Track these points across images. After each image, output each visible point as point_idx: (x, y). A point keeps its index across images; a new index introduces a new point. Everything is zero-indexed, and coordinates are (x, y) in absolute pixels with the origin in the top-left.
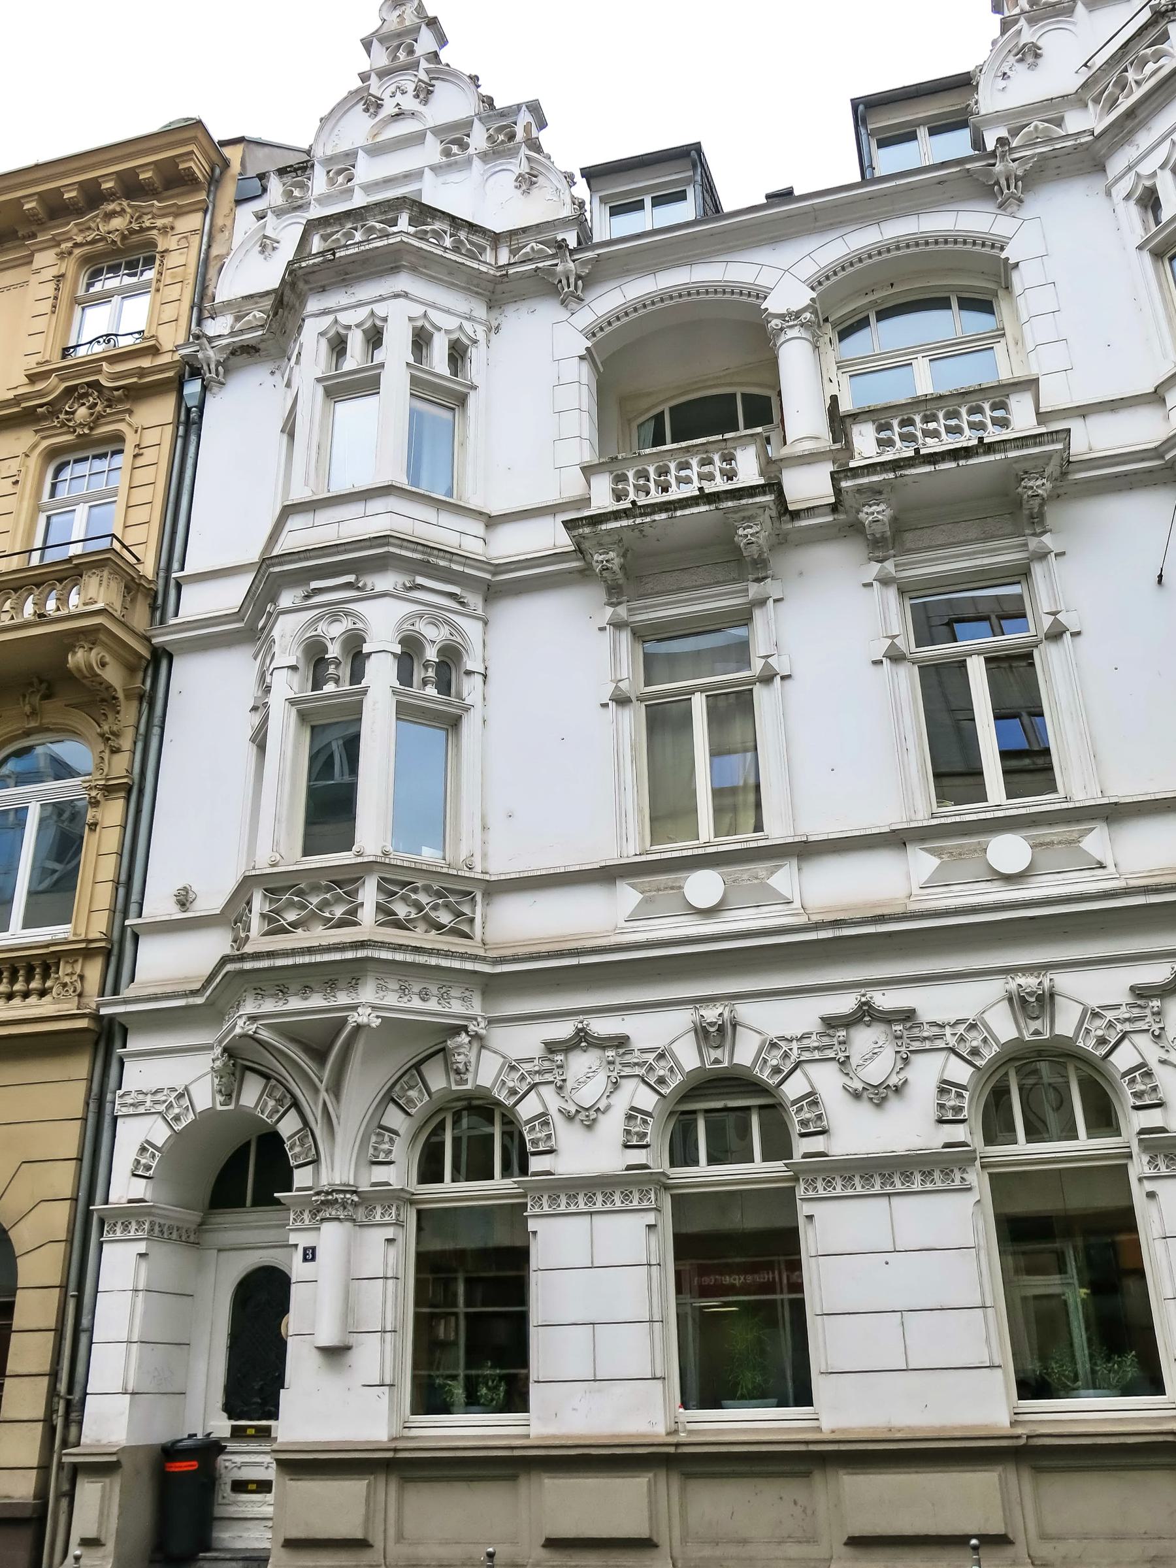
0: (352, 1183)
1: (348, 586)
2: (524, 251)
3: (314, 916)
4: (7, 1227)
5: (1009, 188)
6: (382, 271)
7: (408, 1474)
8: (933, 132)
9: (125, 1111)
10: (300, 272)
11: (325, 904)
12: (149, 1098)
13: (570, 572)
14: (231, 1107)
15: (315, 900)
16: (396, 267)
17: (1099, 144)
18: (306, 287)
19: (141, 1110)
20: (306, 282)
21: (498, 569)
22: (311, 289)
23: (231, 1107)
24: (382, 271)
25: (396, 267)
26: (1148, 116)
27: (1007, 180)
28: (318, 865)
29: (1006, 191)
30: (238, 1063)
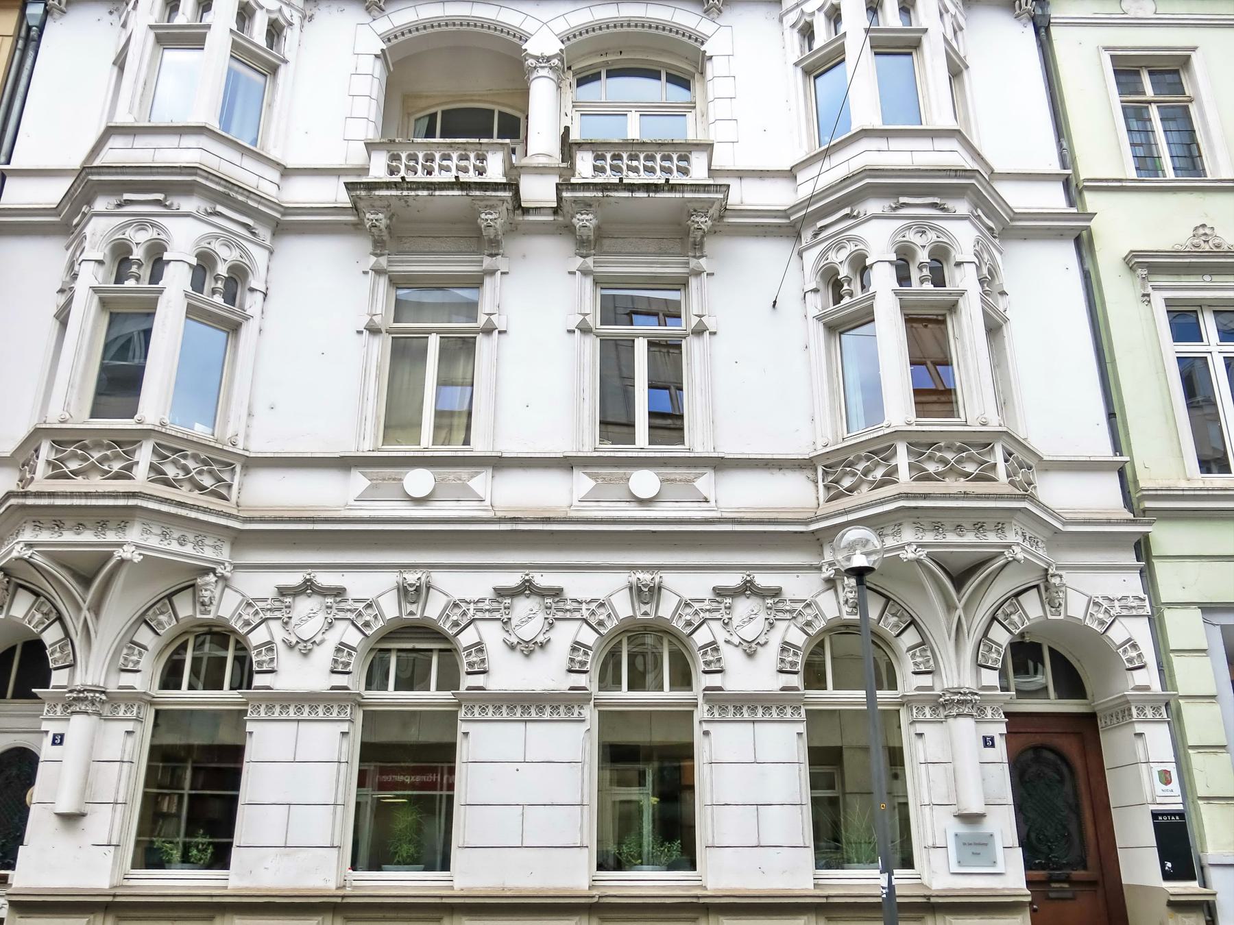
7: (121, 914)
15: (96, 455)
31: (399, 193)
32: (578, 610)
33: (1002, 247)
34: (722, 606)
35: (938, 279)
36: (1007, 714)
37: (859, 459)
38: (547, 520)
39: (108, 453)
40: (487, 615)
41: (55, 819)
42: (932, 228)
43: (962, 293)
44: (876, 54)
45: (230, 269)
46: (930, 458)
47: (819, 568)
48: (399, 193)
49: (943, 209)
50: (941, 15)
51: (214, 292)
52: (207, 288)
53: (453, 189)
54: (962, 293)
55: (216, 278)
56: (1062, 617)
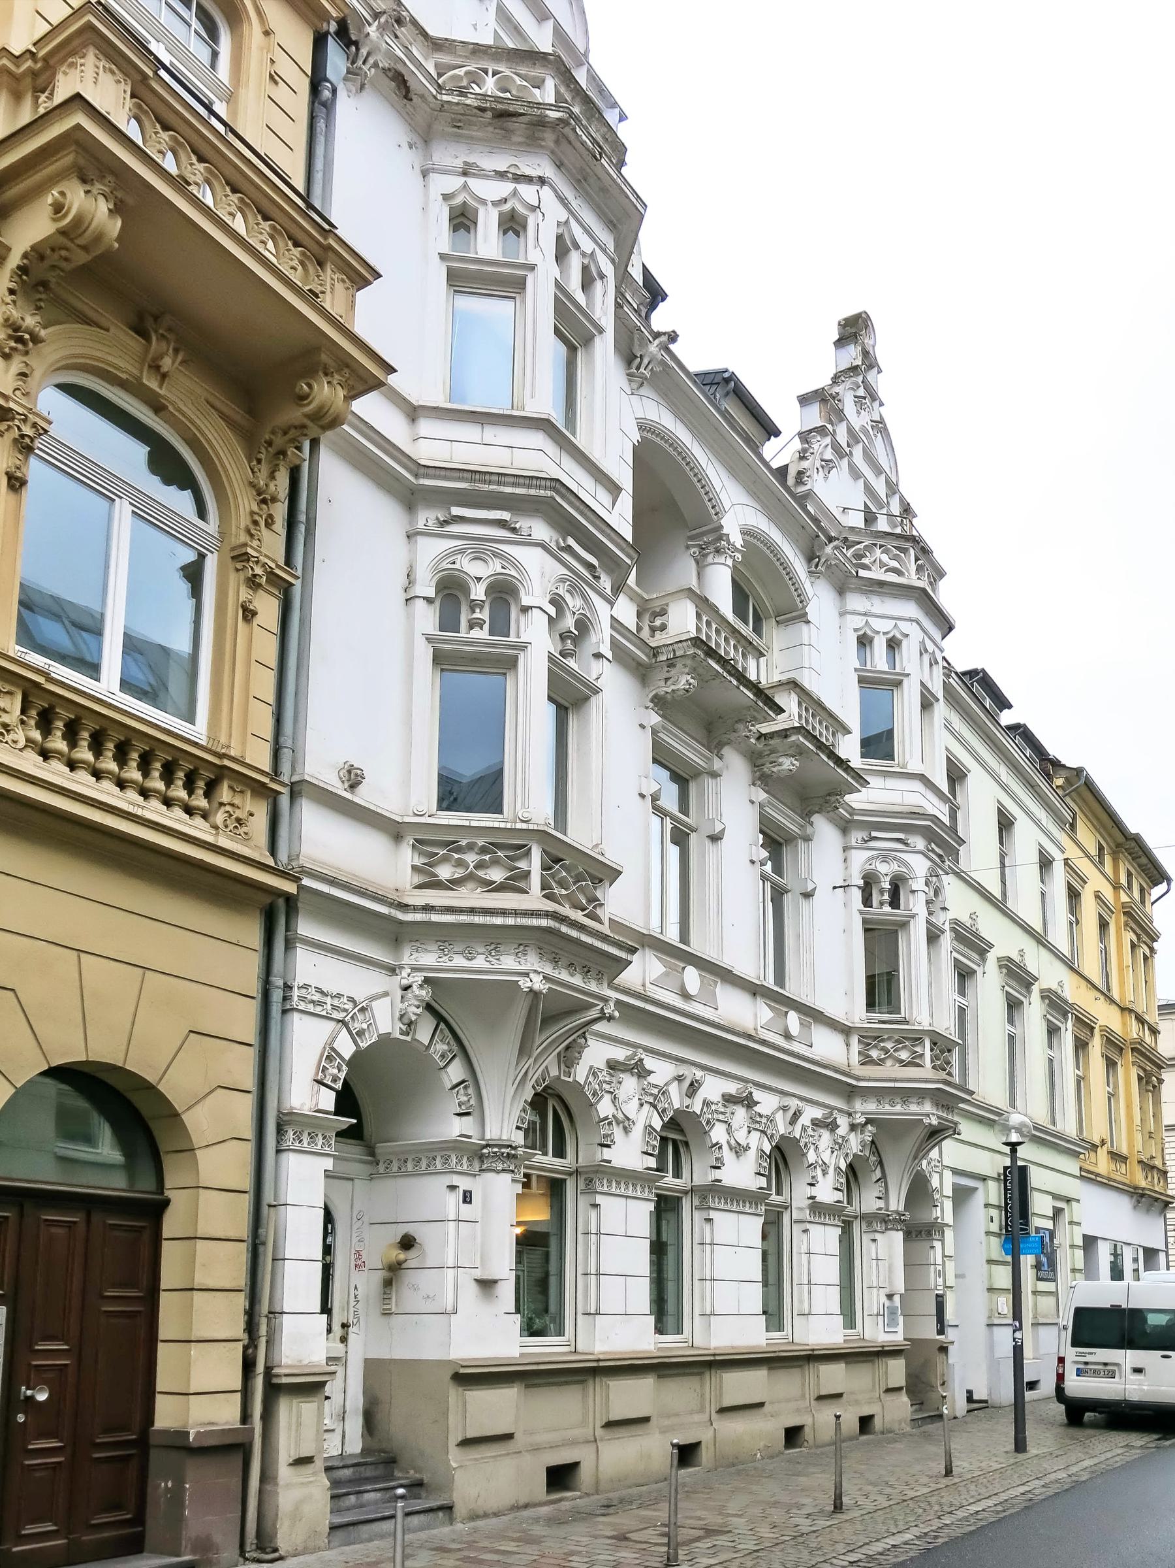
0: (504, 1138)
1: (501, 524)
2: (456, 72)
3: (470, 877)
4: (179, 1108)
5: (364, 63)
6: (605, 214)
7: (662, 1373)
8: (1003, 703)
9: (302, 1006)
10: (567, 130)
11: (480, 865)
12: (328, 1000)
13: (634, 658)
14: (408, 1038)
15: (471, 858)
16: (615, 226)
17: (854, 580)
18: (552, 145)
19: (318, 1010)
20: (557, 142)
21: (420, 470)
22: (553, 152)
23: (408, 1038)
24: (605, 214)
25: (615, 226)
26: (480, 139)
27: (369, 54)
28: (483, 824)
29: (642, 370)
30: (443, 1005)
31: (721, 671)
32: (321, 1004)
33: (86, 224)
34: (614, 1080)
35: (895, 902)
36: (658, 1195)
37: (470, 847)
38: (333, 882)
39: (487, 857)
40: (311, 1008)
41: (474, 1285)
42: (584, 597)
43: (523, 647)
44: (1085, 882)
45: (490, 590)
46: (875, 1046)
47: (393, 970)
48: (721, 671)
49: (906, 844)
50: (921, 654)
51: (882, 904)
52: (875, 903)
53: (750, 690)
54: (523, 647)
55: (882, 891)
56: (570, 1080)
